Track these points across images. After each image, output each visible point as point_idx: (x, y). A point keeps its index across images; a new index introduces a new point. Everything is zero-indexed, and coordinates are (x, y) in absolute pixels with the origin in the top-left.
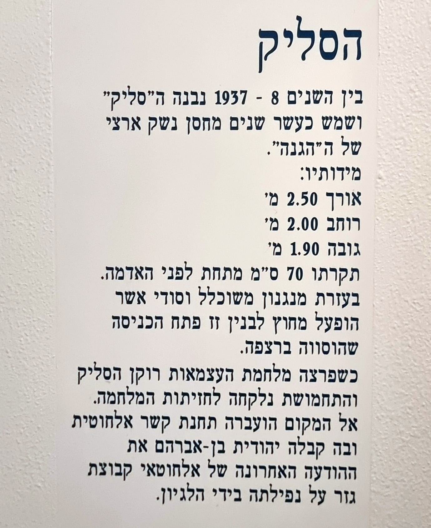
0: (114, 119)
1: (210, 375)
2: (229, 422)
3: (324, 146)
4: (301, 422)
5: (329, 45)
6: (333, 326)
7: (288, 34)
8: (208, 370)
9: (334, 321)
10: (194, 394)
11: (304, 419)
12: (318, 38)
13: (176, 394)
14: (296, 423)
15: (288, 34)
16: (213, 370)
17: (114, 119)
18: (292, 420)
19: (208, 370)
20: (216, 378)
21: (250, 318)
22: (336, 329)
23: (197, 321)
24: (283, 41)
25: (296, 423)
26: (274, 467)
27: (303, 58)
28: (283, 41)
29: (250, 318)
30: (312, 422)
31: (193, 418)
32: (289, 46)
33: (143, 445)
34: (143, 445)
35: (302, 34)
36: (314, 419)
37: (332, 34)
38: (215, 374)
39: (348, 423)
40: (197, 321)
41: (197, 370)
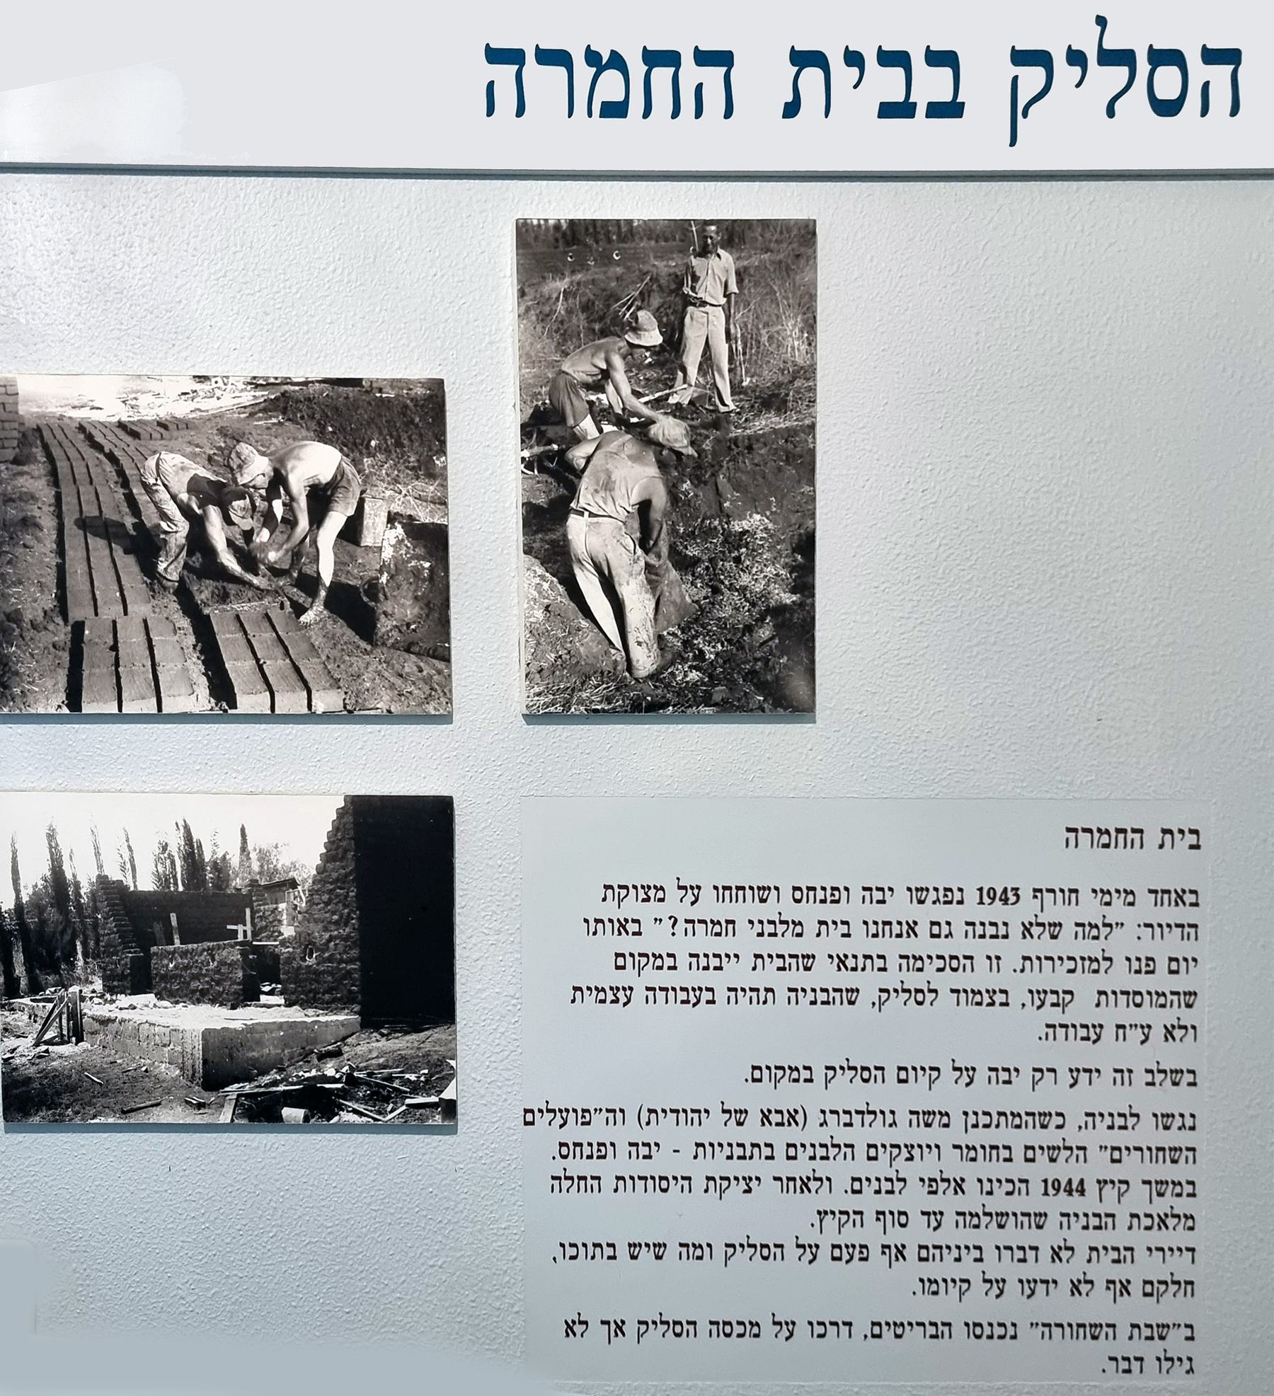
0: (744, 1178)
1: (615, 995)
2: (651, 994)
3: (604, 1114)
4: (637, 958)
5: (1168, 82)
6: (857, 1256)
7: (1076, 58)
8: (611, 988)
9: (858, 1249)
10: (589, 989)
11: (641, 955)
12: (1143, 66)
13: (585, 1245)
14: (630, 960)
15: (1076, 58)
16: (618, 989)
17: (744, 1178)
18: (623, 955)
19: (611, 988)
20: (623, 999)
21: (770, 922)
22: (861, 1259)
23: (865, 1251)
24: (1065, 73)
25: (630, 960)
26: (794, 1179)
27: (1111, 112)
28: (1065, 73)
29: (770, 922)
30: (652, 959)
31: (876, 923)
32: (1078, 85)
33: (912, 928)
34: (912, 928)
35: (1108, 57)
36: (654, 955)
37: (1174, 58)
38: (621, 994)
39: (953, 1184)
40: (865, 1251)
41: (655, 887)
